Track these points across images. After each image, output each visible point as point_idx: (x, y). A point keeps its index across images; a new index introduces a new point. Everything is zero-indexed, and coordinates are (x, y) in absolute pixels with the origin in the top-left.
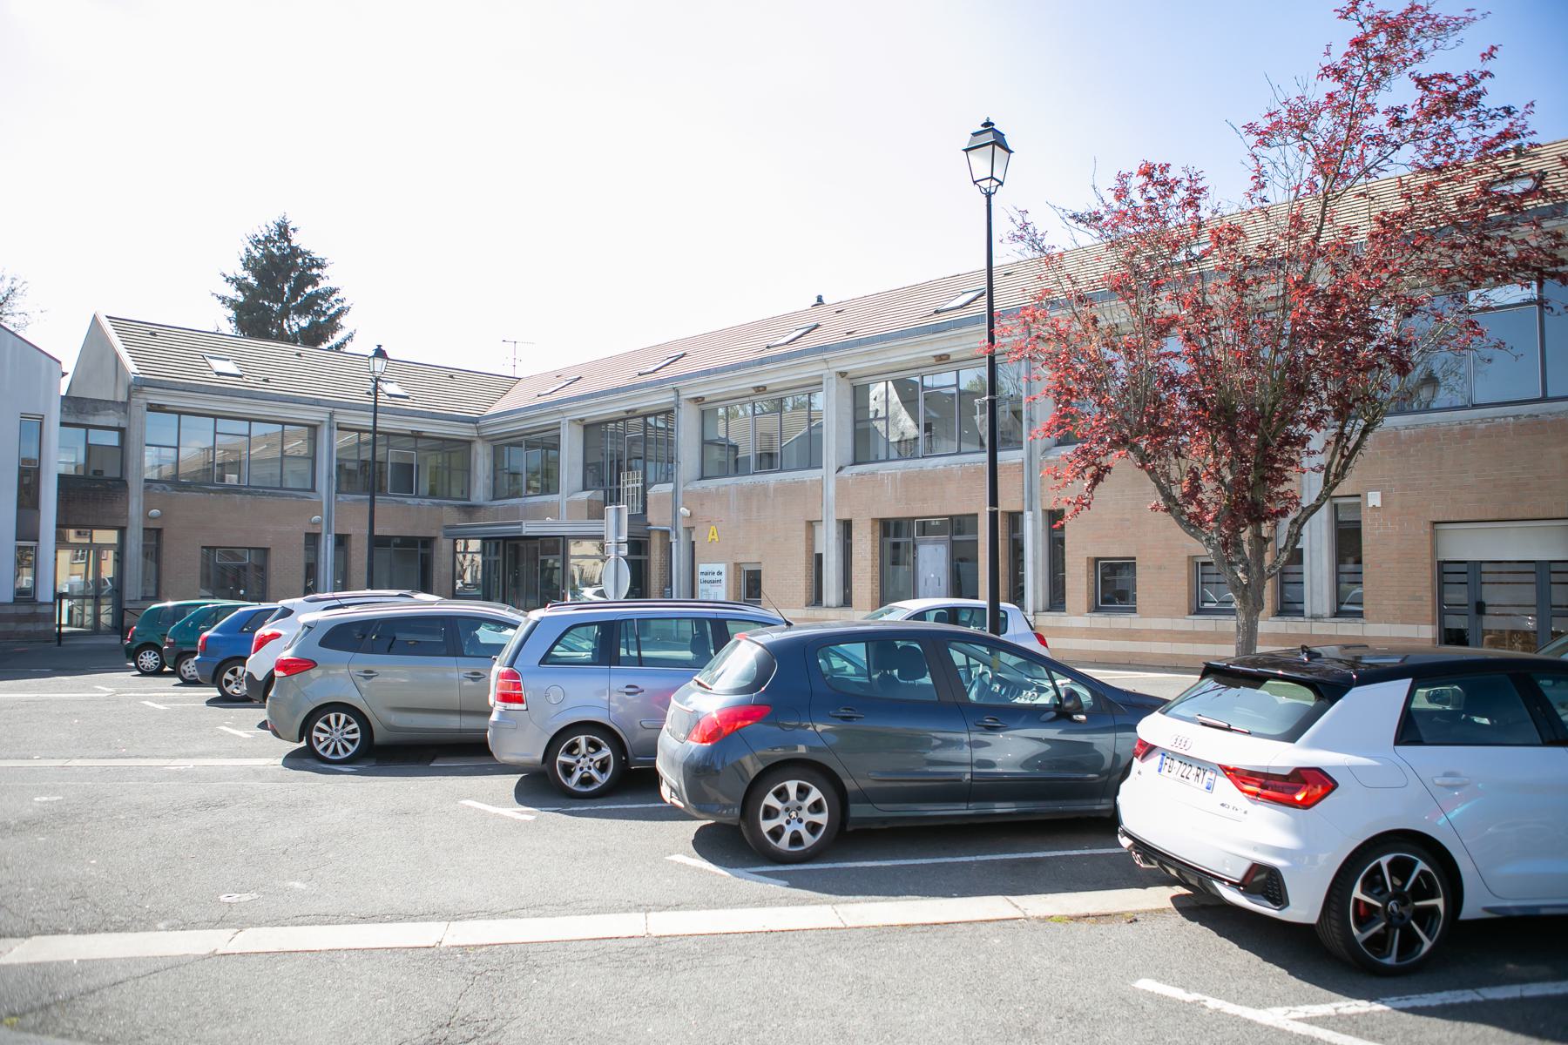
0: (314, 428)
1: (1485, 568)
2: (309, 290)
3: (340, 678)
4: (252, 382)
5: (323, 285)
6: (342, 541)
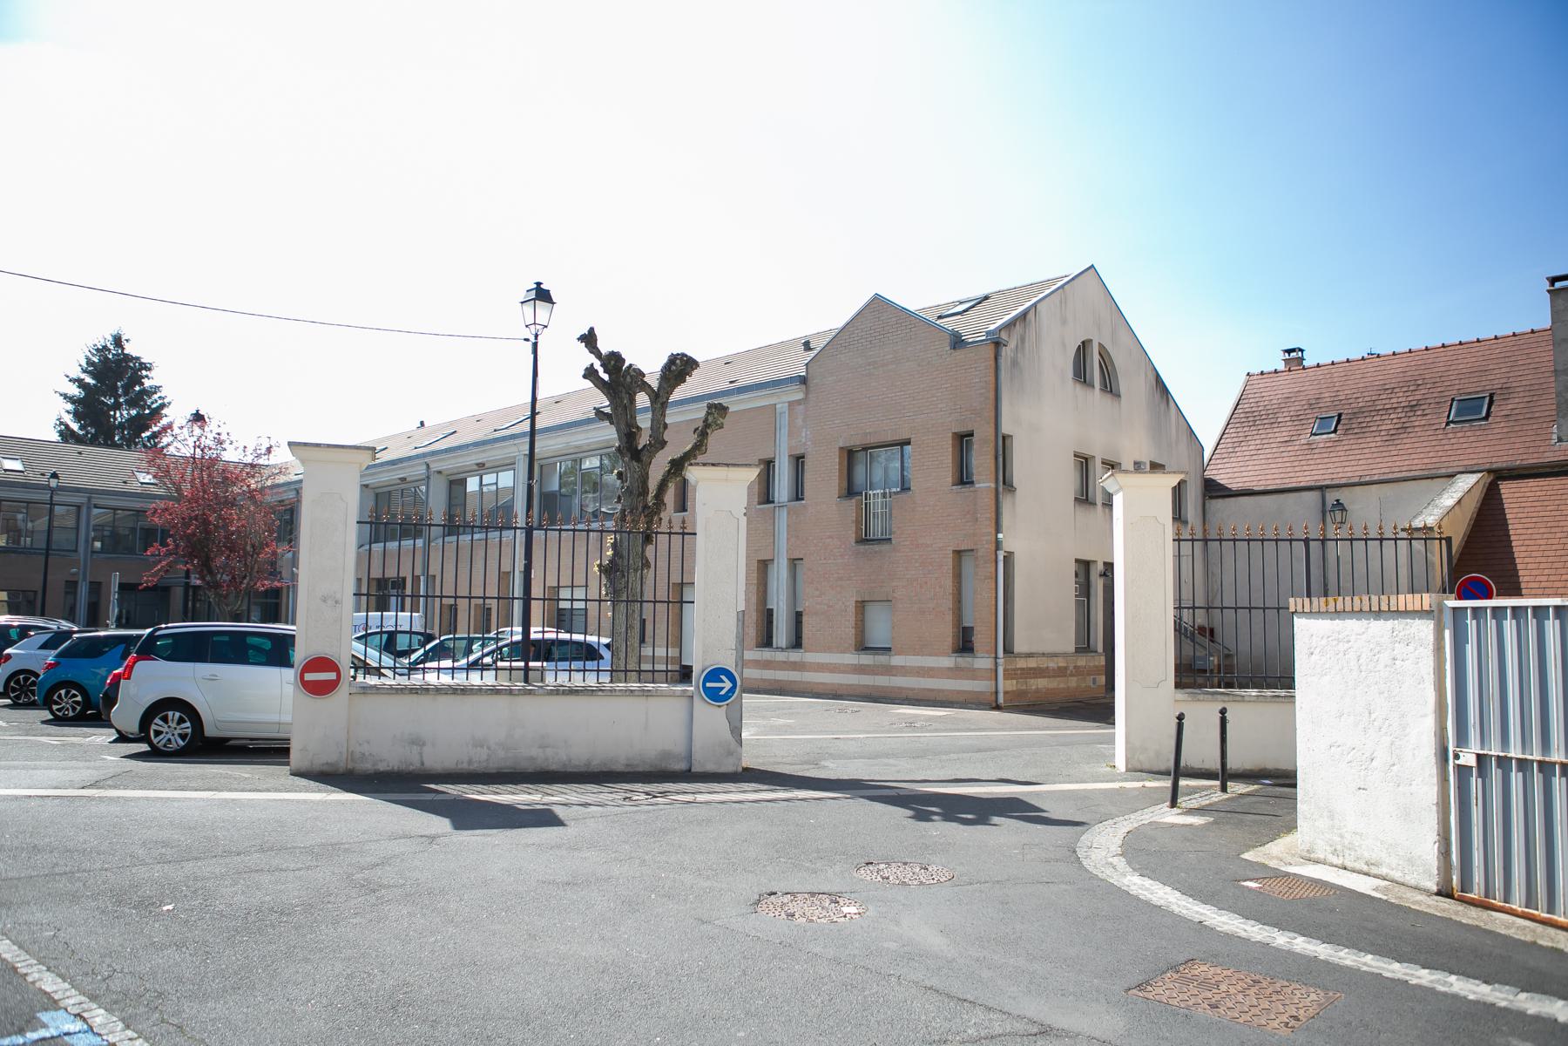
0: (79, 507)
5: (147, 383)
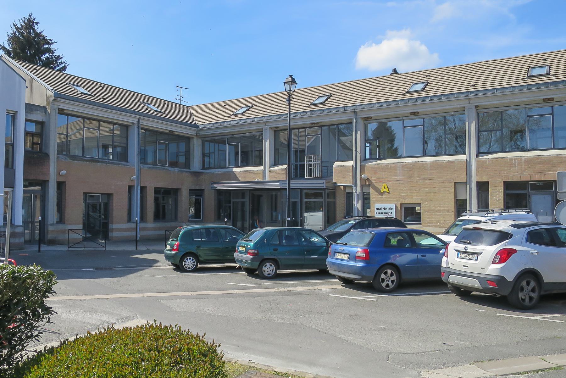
6: (143, 189)
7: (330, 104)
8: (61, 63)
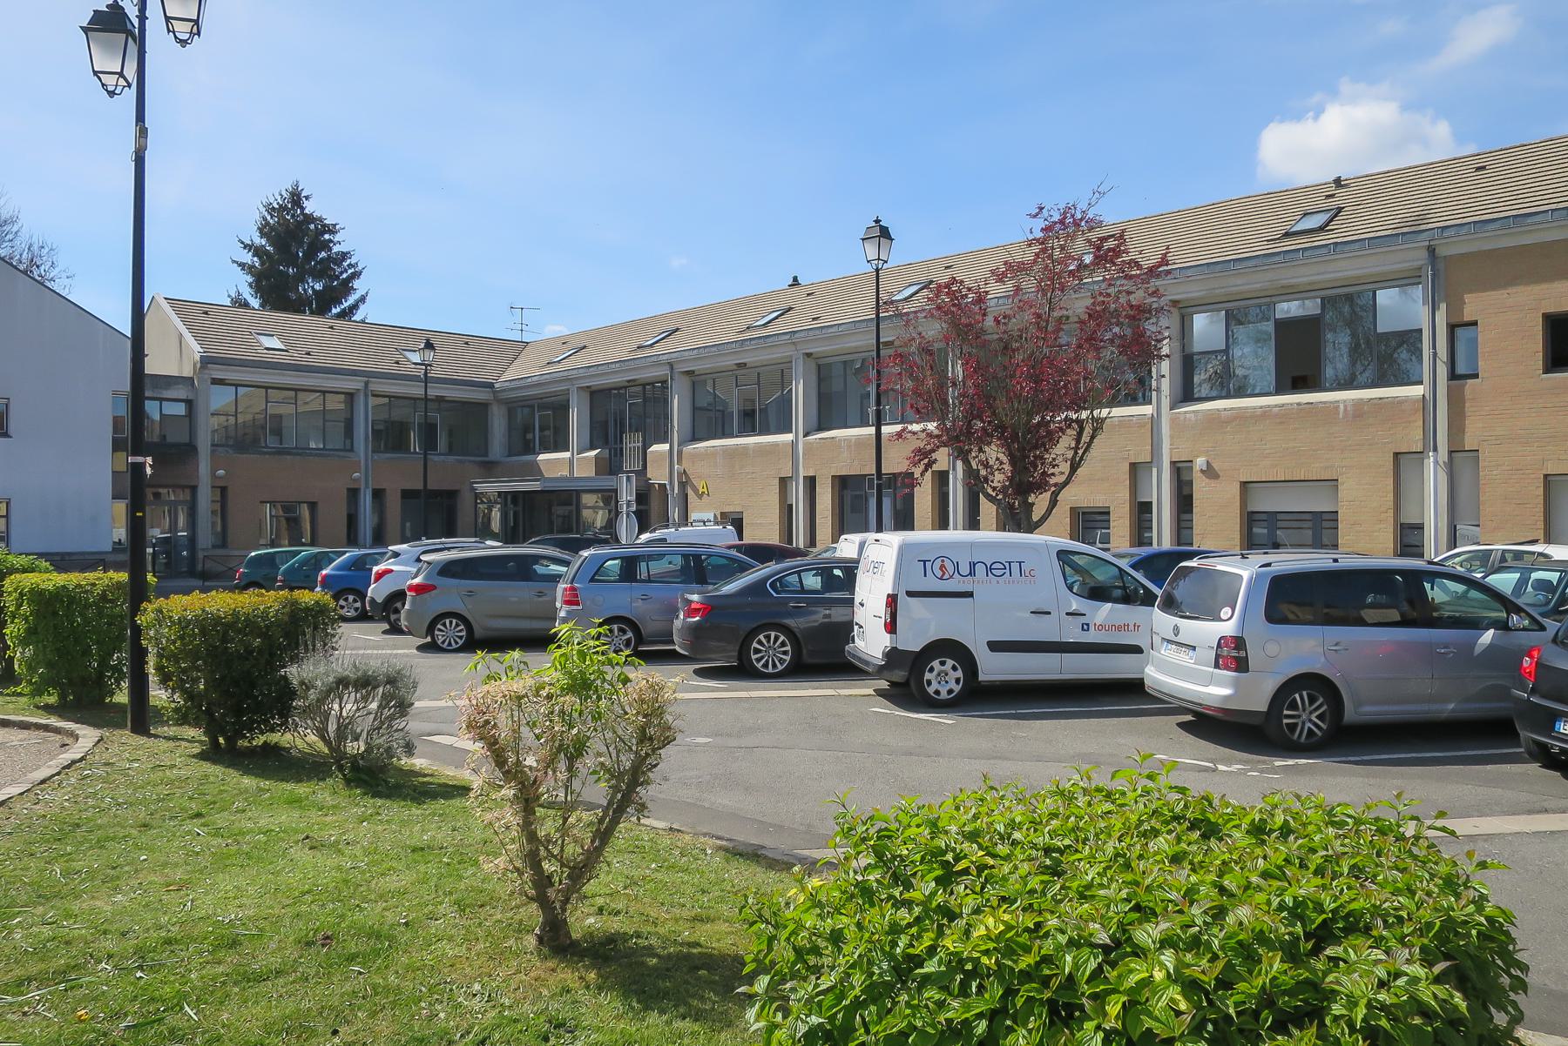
0: (350, 396)
1: (1279, 517)
2: (323, 254)
3: (453, 595)
4: (295, 357)
6: (378, 494)
7: (1343, 231)
8: (350, 266)
